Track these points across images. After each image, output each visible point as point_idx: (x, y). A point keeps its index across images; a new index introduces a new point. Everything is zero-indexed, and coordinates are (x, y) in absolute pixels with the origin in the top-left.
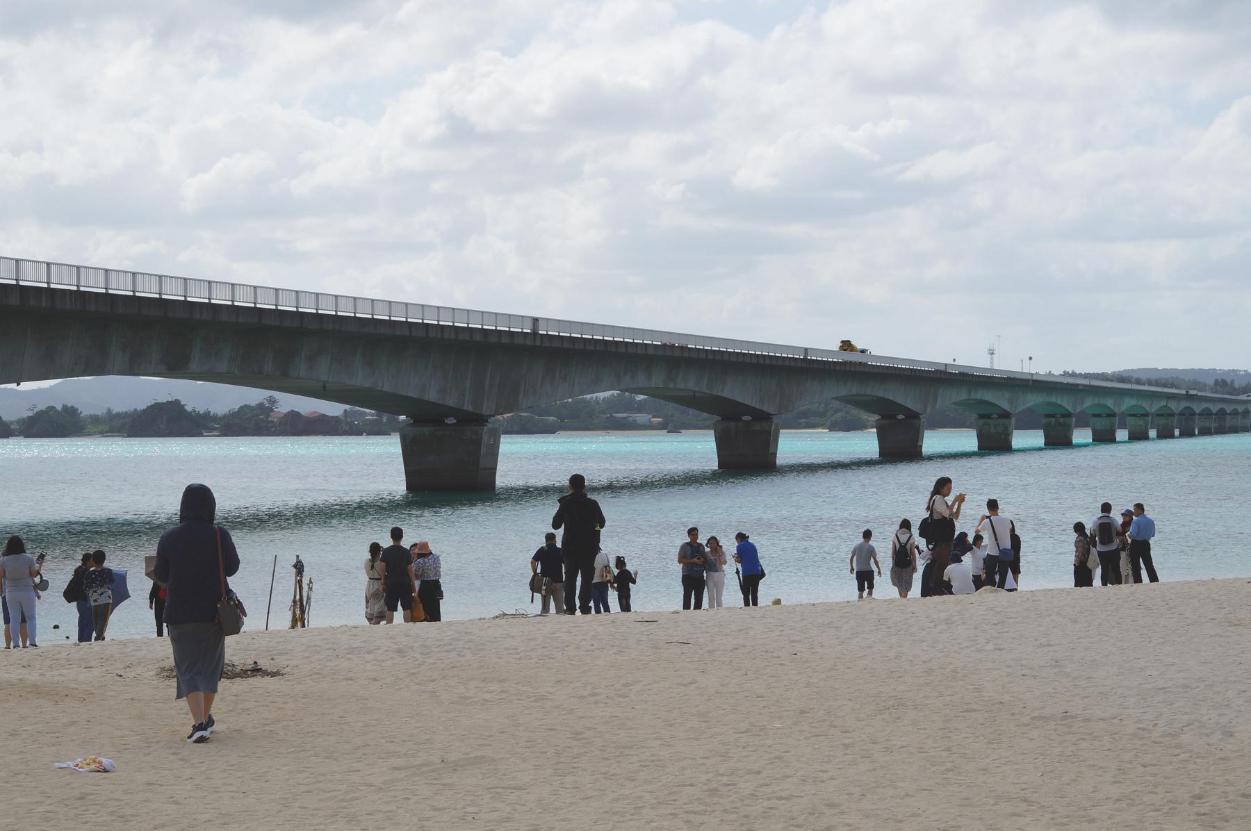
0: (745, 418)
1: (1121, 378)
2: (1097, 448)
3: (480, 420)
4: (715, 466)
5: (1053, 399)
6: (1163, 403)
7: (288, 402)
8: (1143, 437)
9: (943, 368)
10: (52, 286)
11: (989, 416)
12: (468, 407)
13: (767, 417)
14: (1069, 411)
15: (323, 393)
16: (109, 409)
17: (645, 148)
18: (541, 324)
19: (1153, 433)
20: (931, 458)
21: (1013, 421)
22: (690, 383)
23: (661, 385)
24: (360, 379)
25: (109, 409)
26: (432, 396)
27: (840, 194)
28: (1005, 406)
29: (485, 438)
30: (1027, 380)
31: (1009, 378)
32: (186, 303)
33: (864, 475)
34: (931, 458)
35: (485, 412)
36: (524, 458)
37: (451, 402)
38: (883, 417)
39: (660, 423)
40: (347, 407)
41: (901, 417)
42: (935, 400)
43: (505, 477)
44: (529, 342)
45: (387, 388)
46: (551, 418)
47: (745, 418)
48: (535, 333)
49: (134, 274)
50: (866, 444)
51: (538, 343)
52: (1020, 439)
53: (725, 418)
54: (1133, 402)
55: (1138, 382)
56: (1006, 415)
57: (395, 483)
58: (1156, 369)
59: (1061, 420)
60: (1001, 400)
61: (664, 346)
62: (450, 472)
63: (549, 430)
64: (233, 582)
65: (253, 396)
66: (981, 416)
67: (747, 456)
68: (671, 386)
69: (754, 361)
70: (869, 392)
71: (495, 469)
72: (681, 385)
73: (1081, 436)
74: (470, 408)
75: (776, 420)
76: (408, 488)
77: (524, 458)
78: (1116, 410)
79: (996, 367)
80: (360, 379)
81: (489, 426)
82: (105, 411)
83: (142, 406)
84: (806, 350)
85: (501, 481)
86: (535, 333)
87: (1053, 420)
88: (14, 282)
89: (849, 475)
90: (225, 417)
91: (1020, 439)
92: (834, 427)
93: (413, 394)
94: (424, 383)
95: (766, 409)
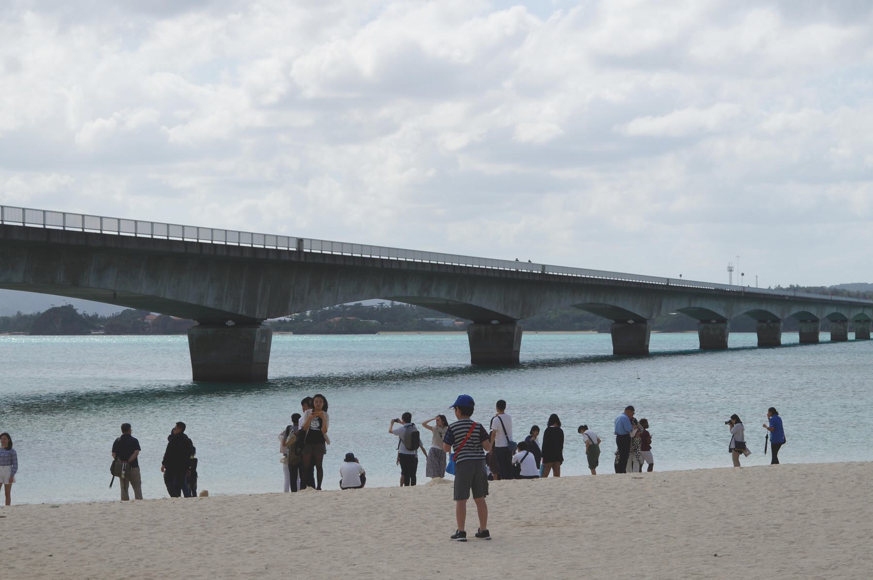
0: (494, 322)
1: (835, 291)
2: (834, 345)
3: (256, 323)
4: (611, 353)
5: (764, 307)
6: (860, 311)
7: (84, 307)
8: (844, 339)
9: (740, 290)
10: (27, 225)
11: (709, 322)
12: (242, 312)
13: (511, 322)
14: (716, 315)
15: (113, 299)
16: (19, 313)
17: (447, 113)
18: (305, 243)
19: (851, 336)
20: (535, 365)
21: (728, 326)
22: (442, 294)
23: (416, 295)
24: (145, 288)
25: (19, 313)
26: (209, 302)
27: (597, 144)
28: (722, 313)
29: (258, 338)
30: (740, 292)
31: (716, 290)
32: (119, 237)
33: (749, 355)
34: (535, 365)
35: (258, 315)
36: (290, 353)
37: (227, 307)
38: (617, 322)
39: (461, 326)
40: (125, 308)
41: (631, 322)
42: (660, 308)
43: (524, 355)
44: (293, 259)
45: (169, 296)
46: (374, 321)
47: (494, 322)
48: (299, 251)
49: (24, 209)
50: (691, 340)
51: (303, 259)
52: (734, 339)
53: (477, 322)
54: (834, 310)
55: (849, 295)
56: (722, 320)
57: (182, 372)
58: (866, 284)
59: (772, 325)
60: (718, 308)
61: (715, 290)
62: (229, 367)
63: (372, 331)
64: (185, 432)
65: (58, 301)
66: (703, 321)
67: (631, 347)
68: (425, 295)
69: (497, 275)
70: (601, 301)
71: (267, 364)
72: (433, 294)
73: (789, 337)
74: (244, 313)
75: (519, 324)
76: (194, 379)
77: (290, 353)
78: (819, 317)
79: (734, 284)
80: (145, 288)
81: (261, 327)
82: (15, 314)
83: (42, 311)
84: (544, 266)
85: (273, 373)
86: (299, 251)
87: (765, 325)
88: (42, 226)
89: (675, 359)
90: (109, 319)
91: (734, 339)
92: (295, 333)
93: (192, 301)
94: (206, 294)
95: (509, 314)
